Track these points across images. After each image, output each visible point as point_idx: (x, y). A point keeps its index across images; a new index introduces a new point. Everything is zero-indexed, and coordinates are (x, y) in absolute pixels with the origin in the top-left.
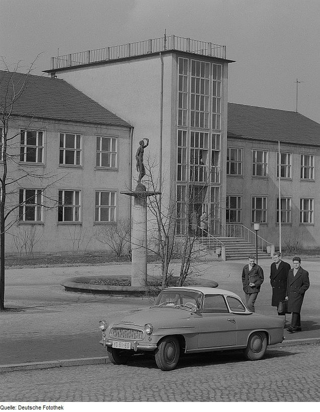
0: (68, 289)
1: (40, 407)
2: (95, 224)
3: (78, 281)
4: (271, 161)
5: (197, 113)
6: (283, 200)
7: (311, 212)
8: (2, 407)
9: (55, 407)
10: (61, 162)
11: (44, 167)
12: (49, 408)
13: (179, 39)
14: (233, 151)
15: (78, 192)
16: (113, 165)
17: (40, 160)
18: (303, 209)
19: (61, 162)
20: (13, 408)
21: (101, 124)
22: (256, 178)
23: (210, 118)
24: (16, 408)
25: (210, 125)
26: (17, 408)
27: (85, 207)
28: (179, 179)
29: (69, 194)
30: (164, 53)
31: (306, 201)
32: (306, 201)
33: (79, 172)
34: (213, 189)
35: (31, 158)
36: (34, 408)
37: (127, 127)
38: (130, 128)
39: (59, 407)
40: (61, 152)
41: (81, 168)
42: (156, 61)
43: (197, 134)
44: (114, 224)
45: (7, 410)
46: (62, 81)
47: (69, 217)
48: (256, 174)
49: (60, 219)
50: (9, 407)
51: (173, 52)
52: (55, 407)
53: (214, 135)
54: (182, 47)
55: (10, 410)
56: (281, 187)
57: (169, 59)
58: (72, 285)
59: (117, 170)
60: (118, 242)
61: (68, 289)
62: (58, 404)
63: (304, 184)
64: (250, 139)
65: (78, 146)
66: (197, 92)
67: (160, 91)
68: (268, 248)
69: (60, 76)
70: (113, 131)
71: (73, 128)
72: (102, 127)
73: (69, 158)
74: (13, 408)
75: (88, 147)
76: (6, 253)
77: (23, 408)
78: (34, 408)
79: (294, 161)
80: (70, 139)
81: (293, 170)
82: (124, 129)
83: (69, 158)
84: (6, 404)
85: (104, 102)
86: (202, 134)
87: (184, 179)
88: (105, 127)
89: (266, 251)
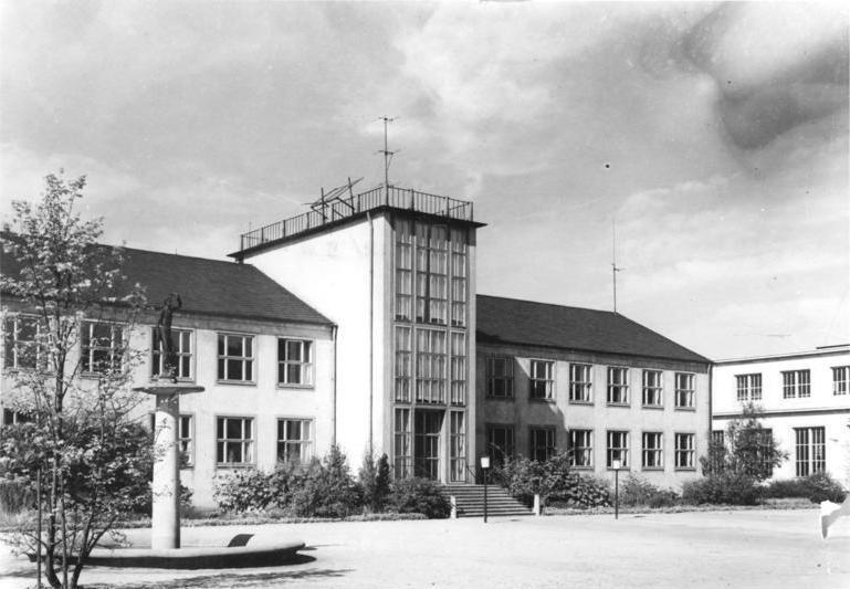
2: (677, 471)
4: (560, 373)
13: (396, 191)
15: (188, 419)
18: (611, 447)
22: (646, 408)
30: (375, 213)
33: (625, 411)
34: (453, 413)
42: (363, 227)
46: (250, 267)
48: (226, 377)
54: (401, 202)
56: (573, 417)
57: (381, 223)
59: (592, 405)
63: (612, 409)
64: (524, 345)
67: (369, 269)
69: (246, 261)
71: (239, 328)
73: (649, 397)
75: (265, 352)
79: (598, 375)
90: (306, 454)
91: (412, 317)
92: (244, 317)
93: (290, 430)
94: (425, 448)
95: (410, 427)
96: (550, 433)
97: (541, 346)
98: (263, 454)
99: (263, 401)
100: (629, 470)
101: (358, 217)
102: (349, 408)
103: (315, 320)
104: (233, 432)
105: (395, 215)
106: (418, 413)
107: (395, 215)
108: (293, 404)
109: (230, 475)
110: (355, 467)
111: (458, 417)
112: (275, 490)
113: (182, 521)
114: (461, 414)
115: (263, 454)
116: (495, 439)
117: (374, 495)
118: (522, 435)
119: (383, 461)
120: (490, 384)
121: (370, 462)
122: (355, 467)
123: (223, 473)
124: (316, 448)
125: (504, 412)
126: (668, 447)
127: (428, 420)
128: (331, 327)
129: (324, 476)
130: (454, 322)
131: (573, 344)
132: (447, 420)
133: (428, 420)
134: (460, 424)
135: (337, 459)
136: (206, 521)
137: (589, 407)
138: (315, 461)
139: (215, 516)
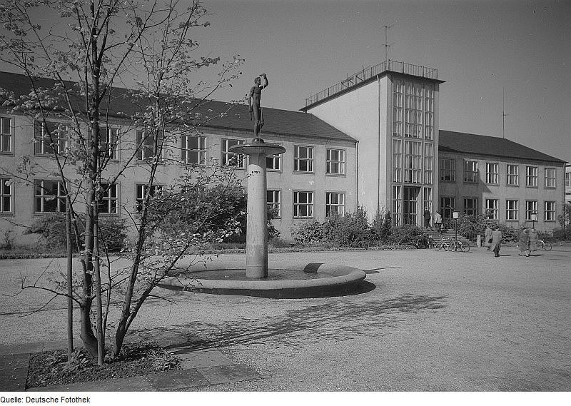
7: (516, 211)
8: (3, 399)
9: (78, 399)
10: (296, 169)
11: (281, 172)
12: (69, 400)
14: (448, 164)
17: (277, 167)
19: (296, 169)
20: (19, 400)
26: (24, 400)
30: (381, 75)
31: (511, 202)
32: (511, 202)
34: (425, 189)
35: (303, 168)
36: (48, 400)
37: (353, 141)
39: (84, 399)
40: (296, 161)
41: (314, 174)
50: (12, 399)
52: (78, 399)
55: (14, 404)
57: (385, 80)
63: (509, 188)
65: (311, 156)
73: (303, 166)
74: (19, 400)
75: (319, 155)
77: (33, 400)
78: (48, 400)
80: (303, 151)
83: (510, 183)
85: (338, 126)
90: (342, 211)
91: (401, 137)
92: (308, 137)
93: (332, 198)
94: (408, 208)
95: (401, 196)
96: (475, 200)
97: (321, 138)
98: (318, 211)
99: (317, 183)
100: (518, 221)
101: (373, 79)
102: (367, 189)
103: (340, 137)
104: (302, 198)
105: (394, 76)
106: (406, 189)
107: (394, 76)
108: (335, 184)
109: (300, 223)
110: (371, 218)
111: (428, 190)
112: (326, 231)
113: (270, 248)
114: (430, 189)
115: (318, 211)
116: (446, 206)
117: (382, 235)
118: (460, 202)
119: (388, 216)
120: (328, 166)
121: (378, 215)
122: (371, 218)
123: (297, 222)
124: (346, 208)
125: (450, 190)
126: (540, 208)
127: (410, 192)
128: (355, 142)
129: (354, 223)
130: (406, 135)
131: (236, 127)
132: (421, 192)
133: (410, 192)
134: (429, 194)
135: (361, 215)
136: (288, 249)
137: (502, 187)
138: (348, 216)
139: (293, 246)
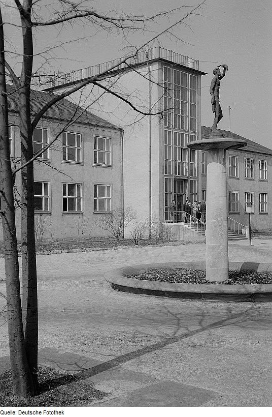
0: (115, 287)
1: (40, 412)
3: (129, 273)
5: (179, 116)
6: (233, 194)
8: (2, 412)
16: (108, 162)
20: (13, 413)
21: (98, 126)
23: (189, 120)
24: (16, 413)
25: (188, 128)
26: (17, 413)
27: (85, 197)
28: (166, 173)
29: (72, 187)
30: (151, 62)
32: (249, 195)
36: (34, 413)
38: (122, 131)
39: (60, 412)
41: (81, 164)
43: (179, 134)
44: (111, 214)
45: (7, 415)
47: (72, 208)
49: (65, 209)
50: (9, 412)
51: (161, 60)
52: (55, 412)
53: (191, 136)
55: (10, 415)
58: (122, 281)
59: (111, 167)
60: (117, 228)
61: (115, 287)
62: (59, 409)
66: (179, 98)
68: (243, 231)
70: (107, 133)
72: (98, 128)
73: (70, 156)
74: (13, 413)
76: (43, 350)
77: (23, 413)
78: (34, 413)
81: (240, 170)
82: (116, 131)
84: (6, 409)
86: (183, 134)
87: (170, 173)
88: (100, 128)
89: (241, 233)
